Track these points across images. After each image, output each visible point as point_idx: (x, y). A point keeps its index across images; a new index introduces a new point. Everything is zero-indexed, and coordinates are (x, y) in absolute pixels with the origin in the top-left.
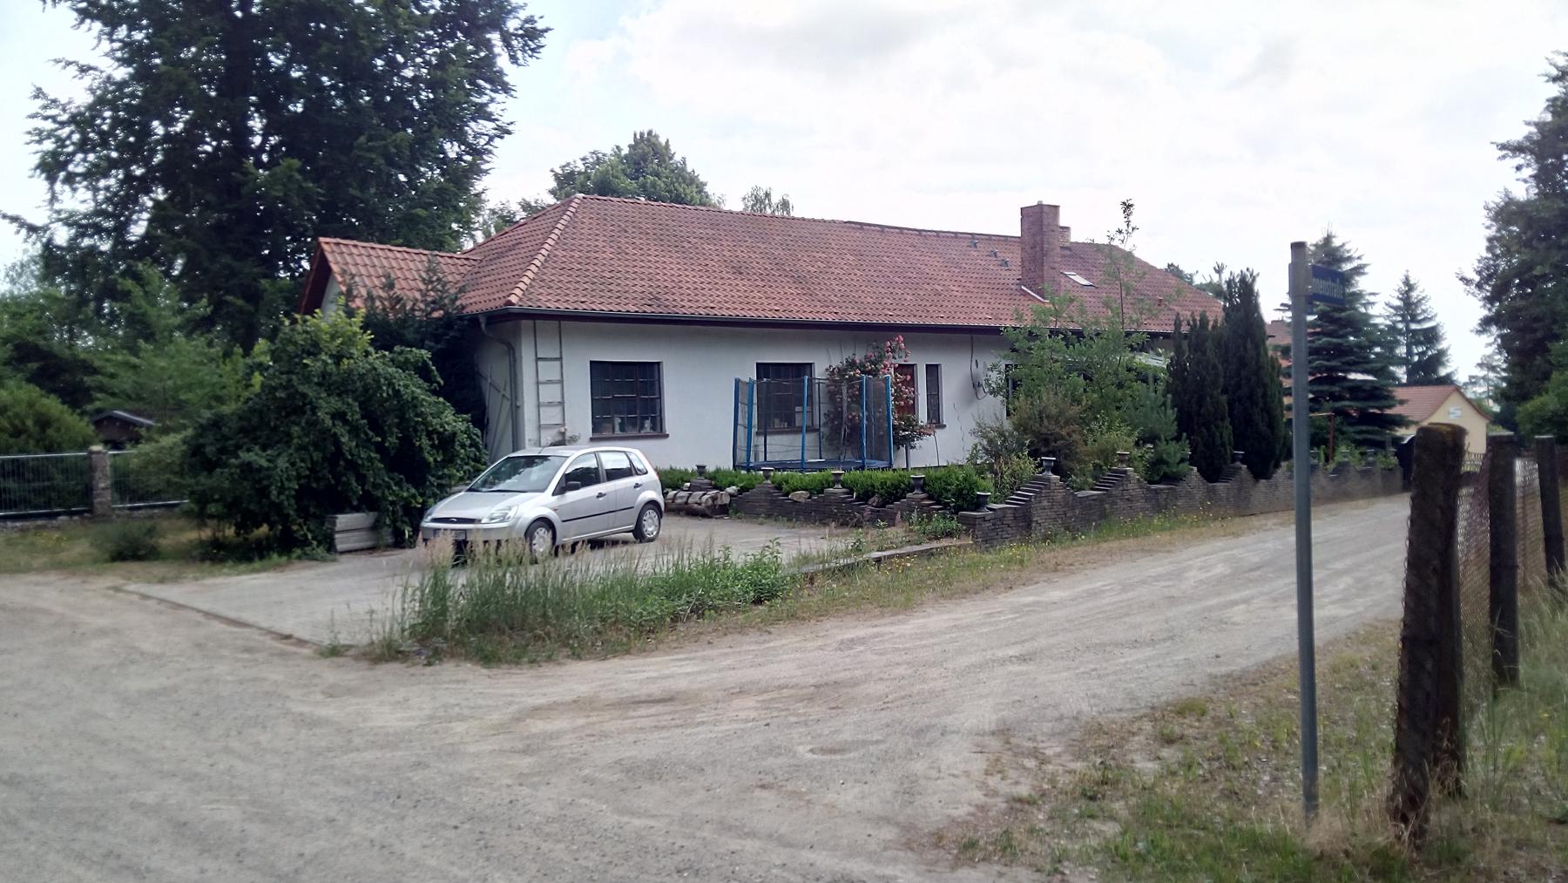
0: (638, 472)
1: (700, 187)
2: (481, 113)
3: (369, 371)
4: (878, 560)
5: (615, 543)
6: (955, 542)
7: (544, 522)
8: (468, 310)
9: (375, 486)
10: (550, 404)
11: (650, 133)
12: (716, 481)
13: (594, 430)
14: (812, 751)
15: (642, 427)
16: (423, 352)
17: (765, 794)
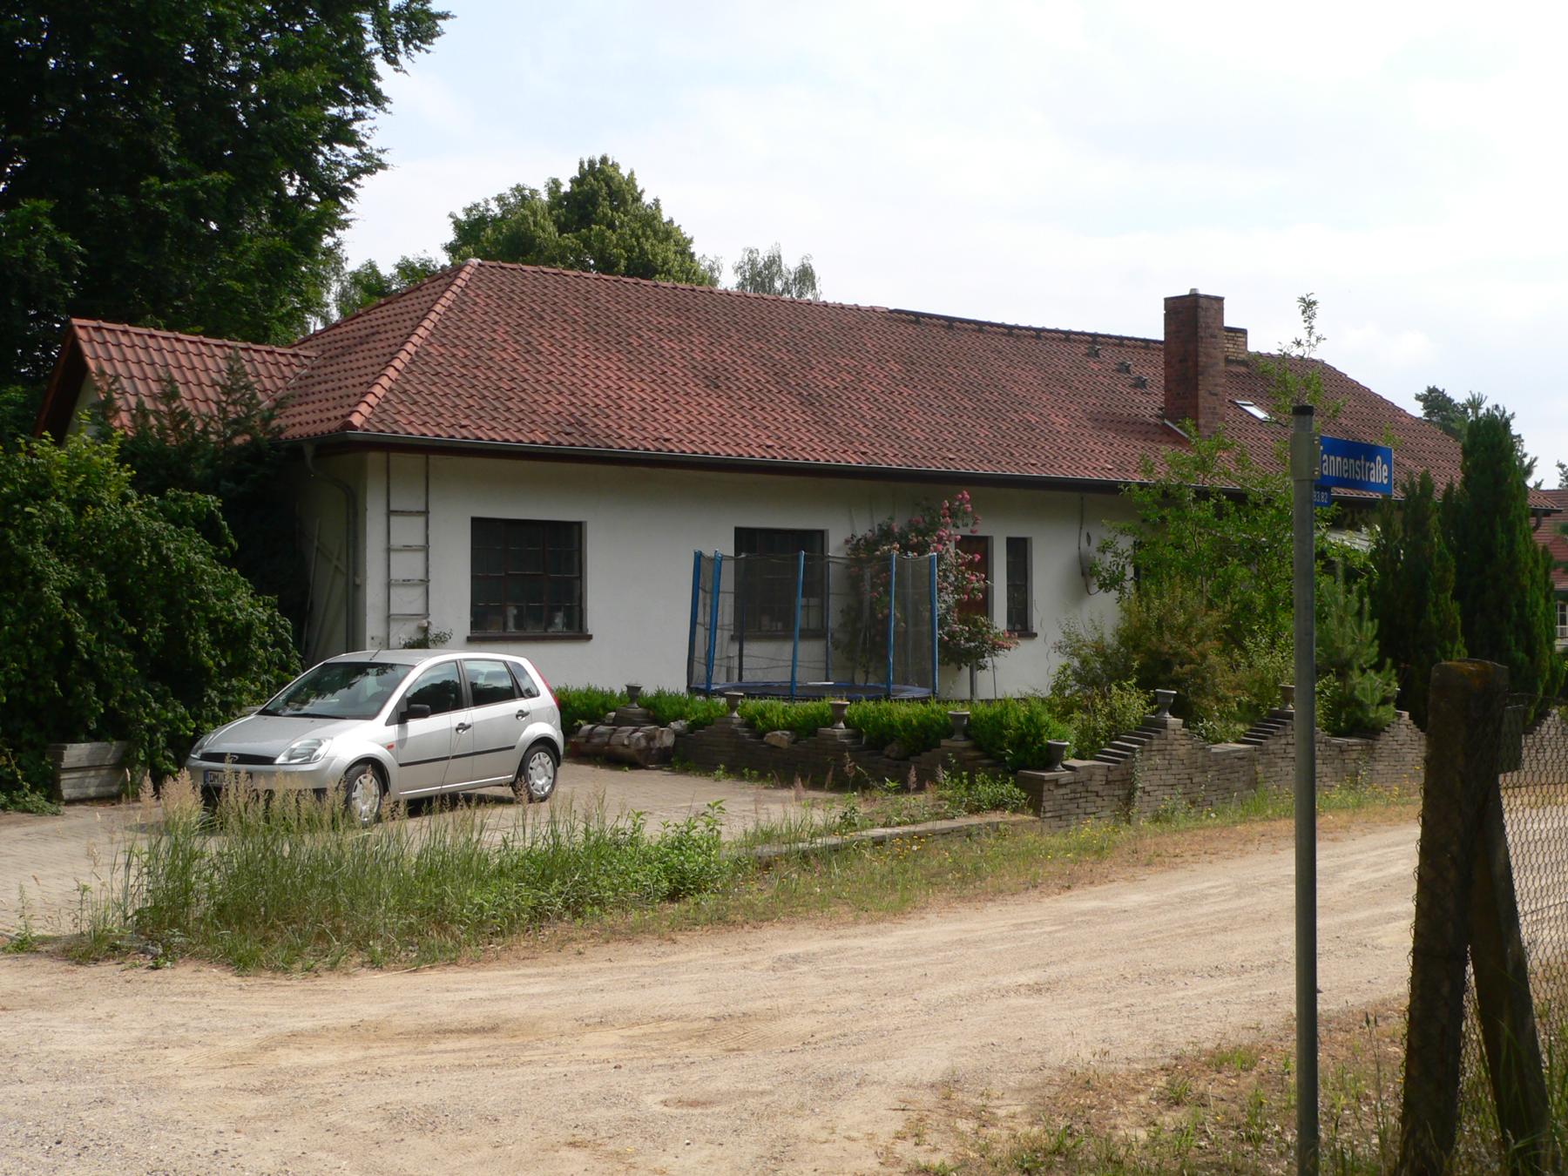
0: (530, 694)
1: (683, 248)
2: (342, 132)
3: (124, 526)
4: (879, 842)
5: (483, 800)
6: (1008, 816)
7: (371, 764)
8: (289, 433)
9: (124, 702)
10: (406, 583)
11: (604, 160)
12: (655, 710)
13: (474, 625)
14: (665, 1103)
15: (550, 623)
16: (211, 498)
17: (573, 1153)
